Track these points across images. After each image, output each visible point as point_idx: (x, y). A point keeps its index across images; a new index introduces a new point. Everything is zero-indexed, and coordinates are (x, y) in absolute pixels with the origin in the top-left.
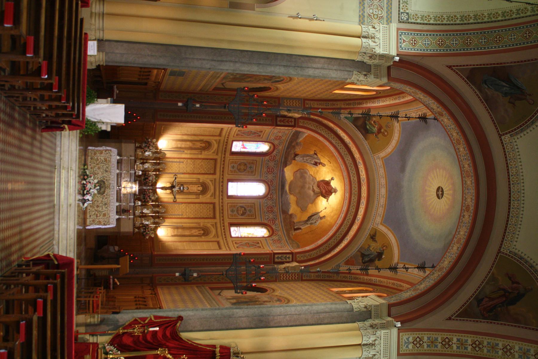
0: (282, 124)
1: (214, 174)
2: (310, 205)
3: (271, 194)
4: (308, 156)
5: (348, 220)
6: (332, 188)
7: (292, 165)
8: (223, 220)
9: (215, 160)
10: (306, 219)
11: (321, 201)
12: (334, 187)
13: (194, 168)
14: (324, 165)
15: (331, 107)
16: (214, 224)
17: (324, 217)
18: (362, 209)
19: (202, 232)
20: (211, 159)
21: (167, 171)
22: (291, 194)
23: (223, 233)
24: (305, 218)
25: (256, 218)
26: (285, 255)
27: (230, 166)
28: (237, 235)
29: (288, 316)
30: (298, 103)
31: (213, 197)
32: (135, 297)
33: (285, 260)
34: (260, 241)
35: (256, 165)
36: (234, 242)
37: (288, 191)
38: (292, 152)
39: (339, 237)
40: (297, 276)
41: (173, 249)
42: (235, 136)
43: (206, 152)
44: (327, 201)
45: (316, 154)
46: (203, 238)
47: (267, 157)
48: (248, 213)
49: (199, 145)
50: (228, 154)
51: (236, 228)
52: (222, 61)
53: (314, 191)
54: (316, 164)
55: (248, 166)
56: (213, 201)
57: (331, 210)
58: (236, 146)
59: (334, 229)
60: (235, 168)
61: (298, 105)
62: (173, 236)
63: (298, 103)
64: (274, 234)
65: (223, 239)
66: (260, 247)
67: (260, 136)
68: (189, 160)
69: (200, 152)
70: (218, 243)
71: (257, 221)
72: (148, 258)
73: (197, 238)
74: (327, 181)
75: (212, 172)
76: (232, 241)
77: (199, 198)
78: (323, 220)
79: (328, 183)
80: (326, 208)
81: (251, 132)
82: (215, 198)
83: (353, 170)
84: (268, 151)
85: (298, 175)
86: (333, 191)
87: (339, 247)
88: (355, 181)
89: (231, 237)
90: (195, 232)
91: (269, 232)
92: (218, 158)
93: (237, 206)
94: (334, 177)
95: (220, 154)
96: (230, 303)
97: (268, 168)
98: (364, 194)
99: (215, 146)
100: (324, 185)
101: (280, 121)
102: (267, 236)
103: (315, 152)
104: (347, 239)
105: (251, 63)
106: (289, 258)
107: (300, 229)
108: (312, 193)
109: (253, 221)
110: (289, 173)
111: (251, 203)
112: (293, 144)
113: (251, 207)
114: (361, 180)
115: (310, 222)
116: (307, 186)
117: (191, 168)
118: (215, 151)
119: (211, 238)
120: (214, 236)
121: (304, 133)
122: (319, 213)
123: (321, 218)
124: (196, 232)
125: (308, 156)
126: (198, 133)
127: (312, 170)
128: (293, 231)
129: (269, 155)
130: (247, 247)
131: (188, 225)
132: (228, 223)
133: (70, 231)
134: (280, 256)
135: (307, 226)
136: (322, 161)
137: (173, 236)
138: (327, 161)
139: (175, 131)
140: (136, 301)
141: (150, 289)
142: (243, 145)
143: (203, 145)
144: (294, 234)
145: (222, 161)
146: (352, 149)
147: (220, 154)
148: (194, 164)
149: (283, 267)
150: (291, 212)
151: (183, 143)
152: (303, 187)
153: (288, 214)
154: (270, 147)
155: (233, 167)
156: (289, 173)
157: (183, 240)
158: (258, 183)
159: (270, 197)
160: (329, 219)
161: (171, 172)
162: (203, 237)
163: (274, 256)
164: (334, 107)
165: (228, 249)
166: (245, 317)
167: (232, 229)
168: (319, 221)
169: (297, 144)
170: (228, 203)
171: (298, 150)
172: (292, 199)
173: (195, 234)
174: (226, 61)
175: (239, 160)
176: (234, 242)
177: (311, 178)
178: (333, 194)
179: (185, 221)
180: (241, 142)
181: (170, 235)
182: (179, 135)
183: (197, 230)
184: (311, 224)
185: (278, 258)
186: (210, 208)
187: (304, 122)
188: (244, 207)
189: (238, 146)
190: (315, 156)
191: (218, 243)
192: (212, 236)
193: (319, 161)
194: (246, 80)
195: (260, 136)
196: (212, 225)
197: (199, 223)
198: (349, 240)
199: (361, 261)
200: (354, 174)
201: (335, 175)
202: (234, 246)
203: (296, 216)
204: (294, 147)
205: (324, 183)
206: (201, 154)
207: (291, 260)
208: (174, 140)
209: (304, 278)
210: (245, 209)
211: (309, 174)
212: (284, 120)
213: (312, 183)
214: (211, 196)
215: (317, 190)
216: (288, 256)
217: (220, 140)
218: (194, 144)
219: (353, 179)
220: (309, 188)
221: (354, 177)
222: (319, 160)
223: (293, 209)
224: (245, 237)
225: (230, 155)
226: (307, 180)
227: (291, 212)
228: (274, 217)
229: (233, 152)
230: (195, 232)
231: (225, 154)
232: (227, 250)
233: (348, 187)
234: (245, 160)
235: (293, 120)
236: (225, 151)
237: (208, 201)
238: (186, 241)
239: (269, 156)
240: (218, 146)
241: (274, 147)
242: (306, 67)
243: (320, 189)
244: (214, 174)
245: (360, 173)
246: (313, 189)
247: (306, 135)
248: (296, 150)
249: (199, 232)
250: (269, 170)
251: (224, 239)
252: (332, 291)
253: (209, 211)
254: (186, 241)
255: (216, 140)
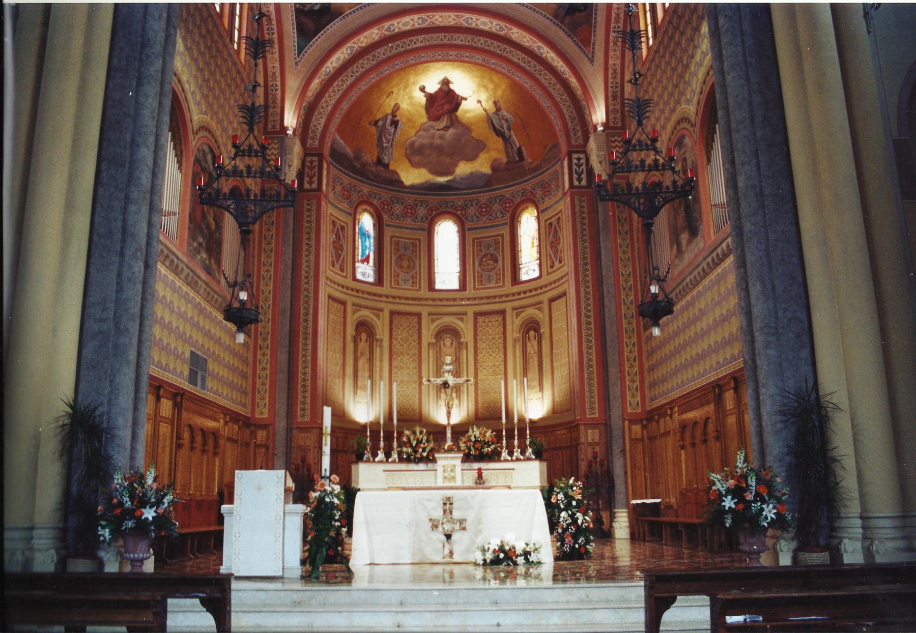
0: (315, 179)
1: (419, 315)
2: (474, 135)
3: (455, 209)
4: (380, 139)
5: (501, 50)
6: (440, 89)
7: (399, 171)
8: (507, 296)
9: (392, 313)
10: (501, 140)
11: (467, 111)
12: (439, 86)
13: (408, 354)
14: (397, 107)
15: (279, 79)
16: (515, 311)
17: (495, 103)
18: (479, 23)
19: (532, 333)
20: (391, 322)
21: (416, 406)
22: (454, 172)
23: (534, 293)
24: (499, 143)
25: (502, 236)
26: (574, 167)
27: (404, 287)
28: (537, 268)
29: (749, 60)
30: (273, 145)
31: (464, 317)
32: (682, 447)
33: (584, 167)
34: (546, 221)
35: (400, 238)
36: (550, 270)
37: (449, 178)
38: (374, 169)
39: (535, 66)
40: (616, 138)
41: (568, 385)
42: (345, 274)
43: (377, 331)
44: (466, 99)
45: (376, 122)
46: (545, 329)
47: (385, 217)
48: (492, 250)
49: (363, 345)
50: (378, 290)
51: (523, 271)
52: (124, 231)
53: (446, 128)
54: (395, 123)
55: (402, 251)
56: (471, 316)
57: (483, 89)
58: (364, 274)
59: (519, 77)
60: (408, 277)
61: (276, 144)
62: (541, 389)
63: (273, 145)
64: (532, 197)
65: (545, 292)
66: (559, 218)
67: (342, 228)
68: (394, 364)
69: (379, 342)
70: (552, 300)
71: (506, 231)
72: (589, 431)
73: (543, 342)
74: (427, 100)
75: (416, 320)
76: (548, 274)
77: (467, 343)
78: (502, 104)
79: (431, 98)
80: (479, 102)
81: (334, 242)
82: (466, 314)
83: (405, 43)
84: (373, 216)
85: (416, 159)
86: (445, 88)
87: (555, 64)
88: (425, 39)
89: (540, 277)
90: (532, 347)
91: (526, 208)
92: (387, 308)
93: (480, 270)
94: (419, 85)
95: (382, 305)
96: (690, 242)
97: (405, 215)
98: (450, 19)
99: (365, 313)
100: (436, 106)
101: (310, 183)
102: (535, 211)
103: (373, 123)
104: (539, 48)
105: (132, 162)
106: (579, 159)
107: (519, 149)
108: (451, 131)
109: (507, 238)
110: (412, 176)
111: (473, 245)
112: (359, 166)
113: (480, 246)
114: (423, 26)
115: (506, 131)
116: (438, 141)
117: (408, 359)
118: (375, 314)
119: (544, 316)
120: (540, 309)
121: (334, 142)
122: (488, 114)
123: (498, 110)
124: (533, 346)
125: (380, 139)
126: (340, 344)
127: (408, 133)
128: (524, 163)
129: (379, 212)
130: (559, 243)
131: (518, 360)
132: (512, 285)
133: (568, 602)
134: (575, 176)
135: (514, 138)
136: (389, 111)
137: (541, 389)
138: (388, 100)
139: (337, 389)
140: (694, 445)
141: (658, 422)
142: (362, 261)
143: (364, 336)
144: (530, 160)
145: (393, 301)
146: (364, 45)
147: (382, 305)
148: (402, 353)
149: (599, 165)
150: (487, 170)
151: (360, 374)
152: (440, 149)
153: (492, 175)
154: (365, 210)
155: (406, 281)
156: (412, 176)
157: (549, 367)
158: (435, 235)
159: (461, 210)
160: (499, 93)
161: (417, 398)
162: (542, 331)
163: (577, 187)
164: (278, 74)
165: (564, 280)
166: (757, 157)
167: (524, 277)
168: (505, 113)
169: (358, 158)
170: (475, 288)
171: (370, 157)
172: (463, 169)
173: (536, 347)
174: (124, 221)
175: (391, 269)
176: (550, 270)
177: (422, 133)
178: (452, 87)
179: (512, 368)
180: (357, 265)
181: (540, 395)
182: (344, 382)
183: (528, 344)
184: (509, 129)
185: (580, 180)
186: (484, 322)
187: (312, 139)
188: (481, 259)
189: (364, 271)
190: (380, 123)
191: (552, 300)
192: (541, 315)
193: (390, 117)
194: (213, 226)
195: (342, 228)
196: (518, 315)
197: (515, 341)
198: (540, 44)
199: (583, 14)
200: (411, 41)
201: (414, 84)
202: (558, 269)
203: (495, 160)
204: (364, 165)
205: (432, 107)
206: (381, 341)
207: (582, 156)
208: (355, 393)
209: (619, 124)
210: (485, 256)
211: (414, 138)
212: (308, 176)
213: (432, 131)
214: (462, 320)
215: (444, 122)
216: (575, 161)
217: (354, 304)
218: (362, 354)
219: (421, 42)
220: (441, 137)
221: (418, 40)
222: (386, 116)
223: (482, 165)
224: (540, 252)
225: (382, 286)
226: (426, 141)
227: (487, 170)
228: (498, 201)
229: (375, 280)
230: (532, 347)
231: (381, 296)
232: (568, 280)
233: (438, 53)
234: (391, 257)
235: (309, 159)
236: (375, 295)
237: (471, 325)
238: (552, 361)
239: (383, 214)
240: (367, 308)
241: (365, 202)
242: (142, 36)
243: (443, 115)
244: (419, 315)
245: (408, 28)
246: (442, 129)
247: (338, 137)
248: (370, 161)
249: (532, 338)
250: (410, 215)
251: (544, 289)
252: (648, 55)
253: (490, 324)
254: (552, 361)
255: (354, 312)
